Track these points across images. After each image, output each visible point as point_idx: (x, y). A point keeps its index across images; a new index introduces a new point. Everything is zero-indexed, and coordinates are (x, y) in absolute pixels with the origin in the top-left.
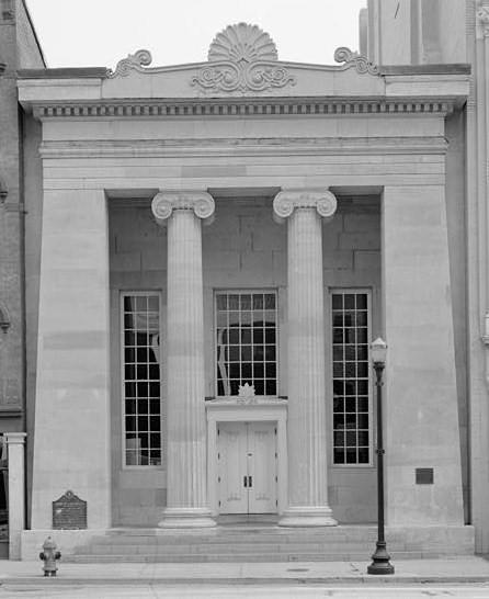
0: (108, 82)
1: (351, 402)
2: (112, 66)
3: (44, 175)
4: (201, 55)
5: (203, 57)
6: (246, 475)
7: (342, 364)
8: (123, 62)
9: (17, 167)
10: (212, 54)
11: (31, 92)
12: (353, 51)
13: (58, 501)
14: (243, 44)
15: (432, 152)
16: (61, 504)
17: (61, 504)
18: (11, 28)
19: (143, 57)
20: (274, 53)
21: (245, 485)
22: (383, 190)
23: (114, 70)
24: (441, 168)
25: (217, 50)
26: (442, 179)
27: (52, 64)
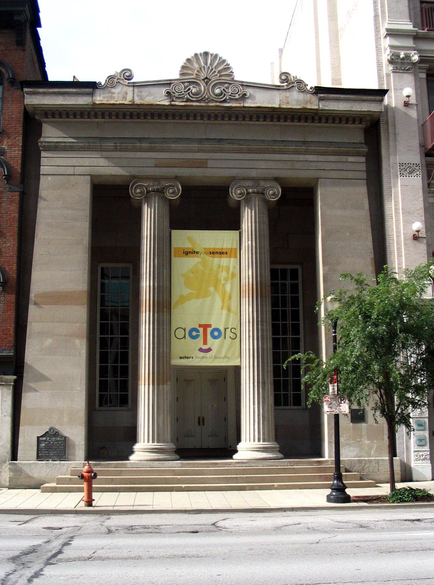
0: (98, 91)
1: (286, 382)
2: (101, 79)
3: (42, 163)
4: (173, 73)
5: (175, 75)
6: (203, 427)
7: (278, 284)
8: (111, 78)
9: (12, 331)
10: (182, 74)
11: (36, 100)
12: (329, 493)
13: (42, 436)
14: (208, 69)
15: (358, 154)
16: (44, 439)
17: (44, 439)
18: (22, 53)
19: (127, 75)
20: (231, 75)
21: (199, 423)
22: (318, 181)
23: (103, 84)
24: (363, 167)
25: (185, 71)
26: (364, 175)
27: (51, 78)
